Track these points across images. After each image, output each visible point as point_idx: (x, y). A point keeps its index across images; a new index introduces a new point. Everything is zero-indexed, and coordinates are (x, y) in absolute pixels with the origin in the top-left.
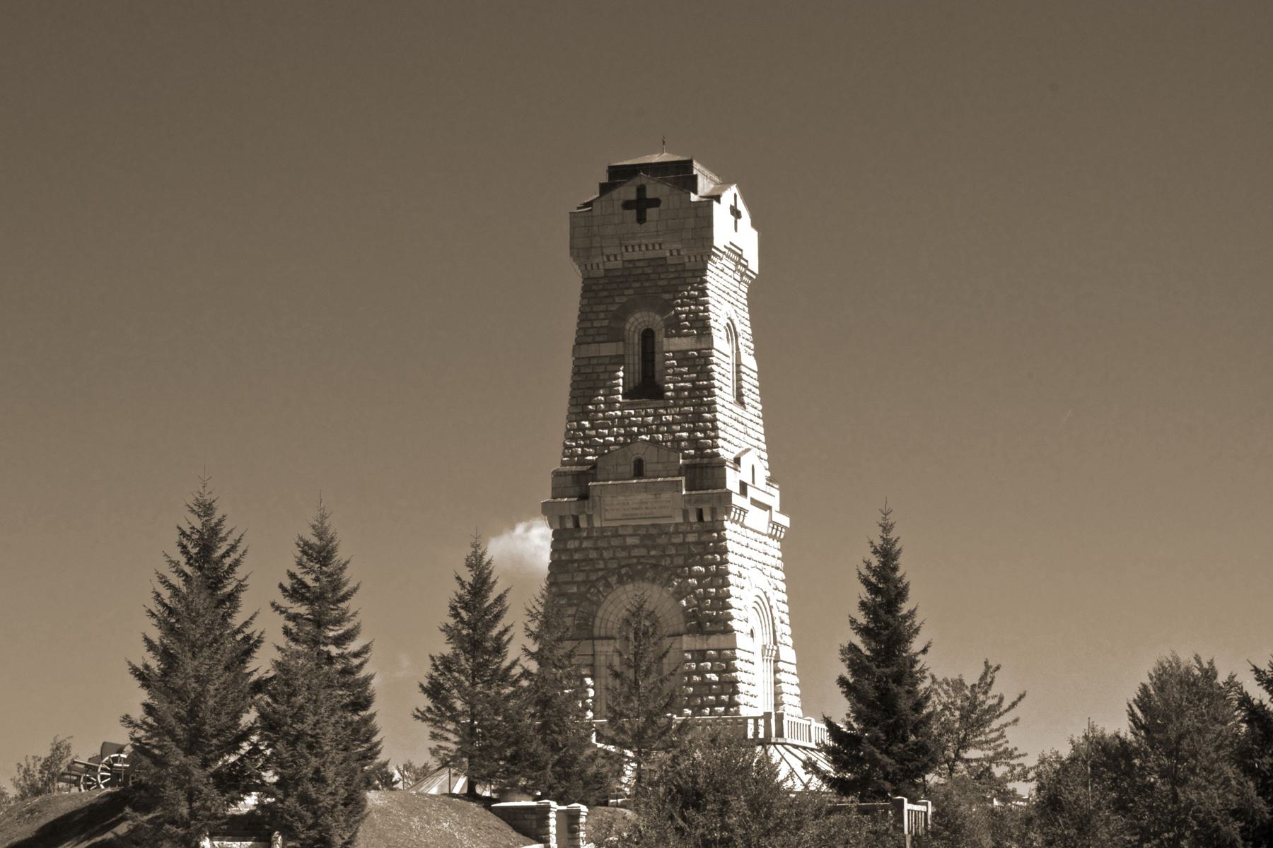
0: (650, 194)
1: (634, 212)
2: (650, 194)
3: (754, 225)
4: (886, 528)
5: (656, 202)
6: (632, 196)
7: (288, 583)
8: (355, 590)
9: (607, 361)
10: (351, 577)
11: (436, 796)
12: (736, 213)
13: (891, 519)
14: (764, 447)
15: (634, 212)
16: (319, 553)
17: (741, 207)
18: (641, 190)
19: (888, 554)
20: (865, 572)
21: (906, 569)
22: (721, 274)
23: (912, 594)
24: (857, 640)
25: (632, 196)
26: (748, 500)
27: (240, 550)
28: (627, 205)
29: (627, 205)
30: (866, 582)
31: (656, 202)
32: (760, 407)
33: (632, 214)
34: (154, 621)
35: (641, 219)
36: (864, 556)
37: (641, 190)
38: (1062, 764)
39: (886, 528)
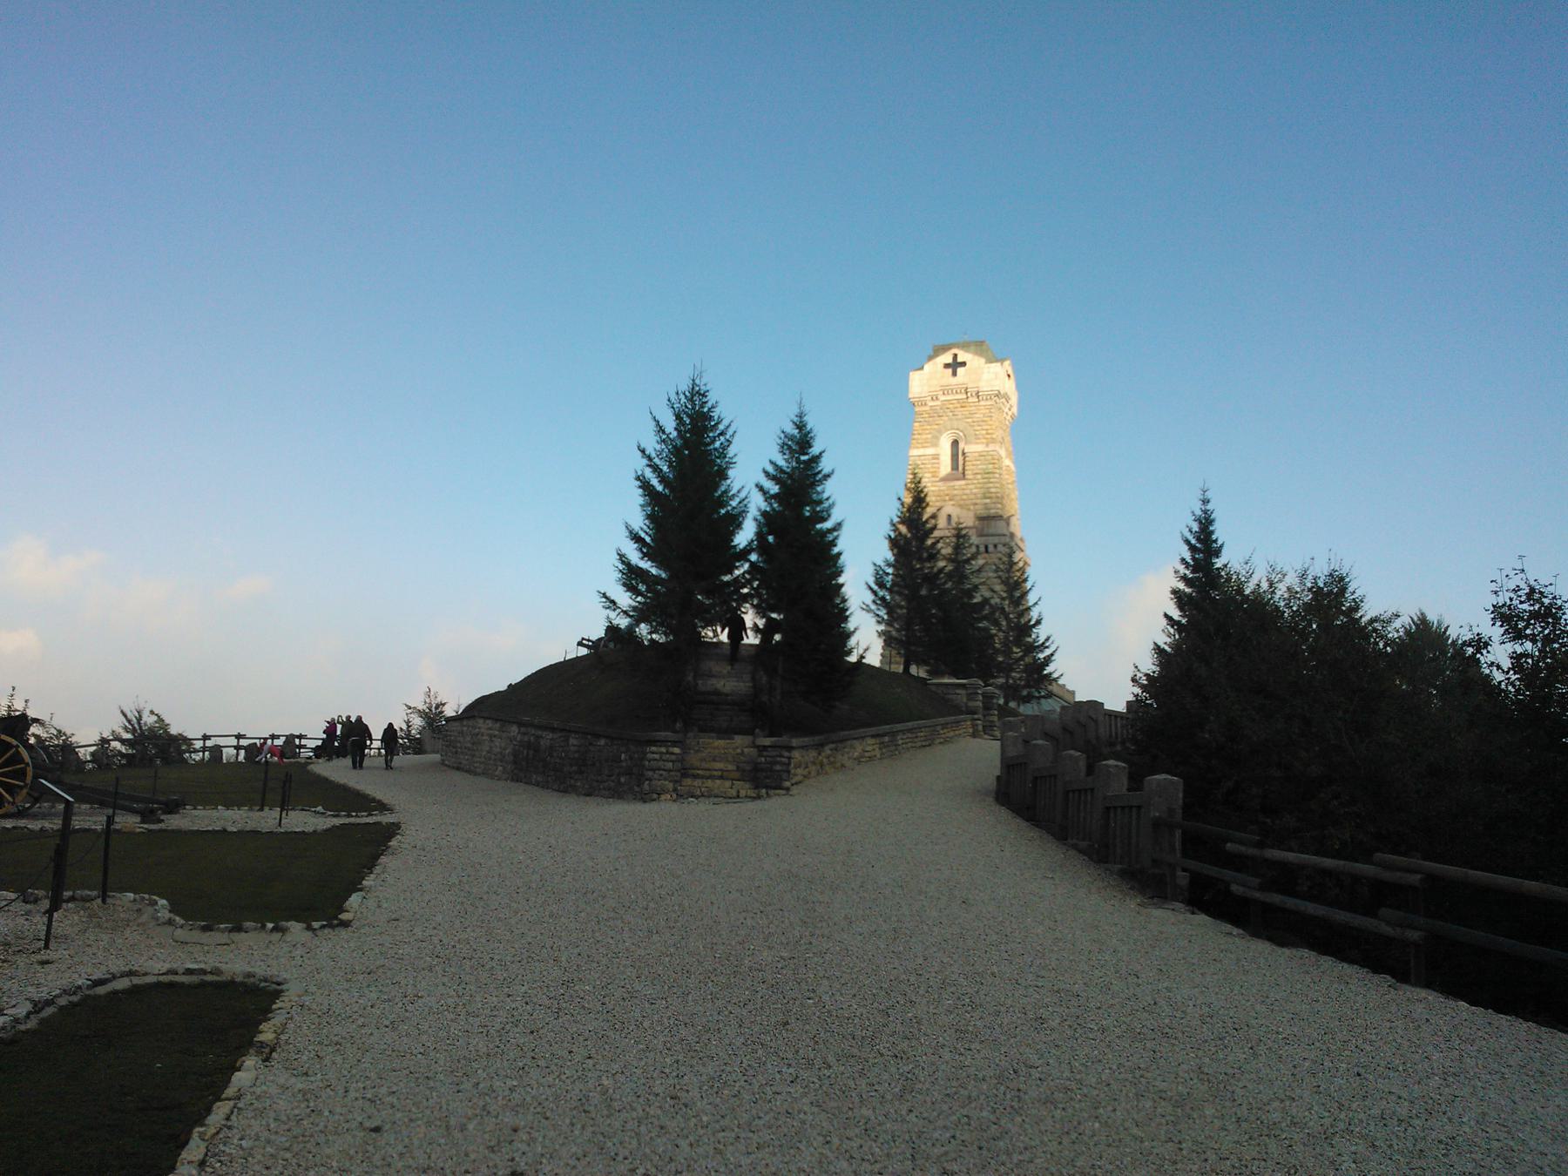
0: (960, 359)
2: (960, 359)
4: (1205, 502)
5: (963, 364)
6: (950, 360)
7: (770, 469)
10: (825, 465)
13: (1209, 495)
16: (800, 442)
18: (955, 356)
19: (1205, 524)
21: (1220, 533)
23: (1224, 551)
24: (1181, 586)
25: (950, 360)
27: (730, 432)
29: (947, 366)
30: (1187, 542)
31: (963, 364)
33: (950, 371)
35: (954, 374)
36: (1185, 523)
39: (1205, 502)
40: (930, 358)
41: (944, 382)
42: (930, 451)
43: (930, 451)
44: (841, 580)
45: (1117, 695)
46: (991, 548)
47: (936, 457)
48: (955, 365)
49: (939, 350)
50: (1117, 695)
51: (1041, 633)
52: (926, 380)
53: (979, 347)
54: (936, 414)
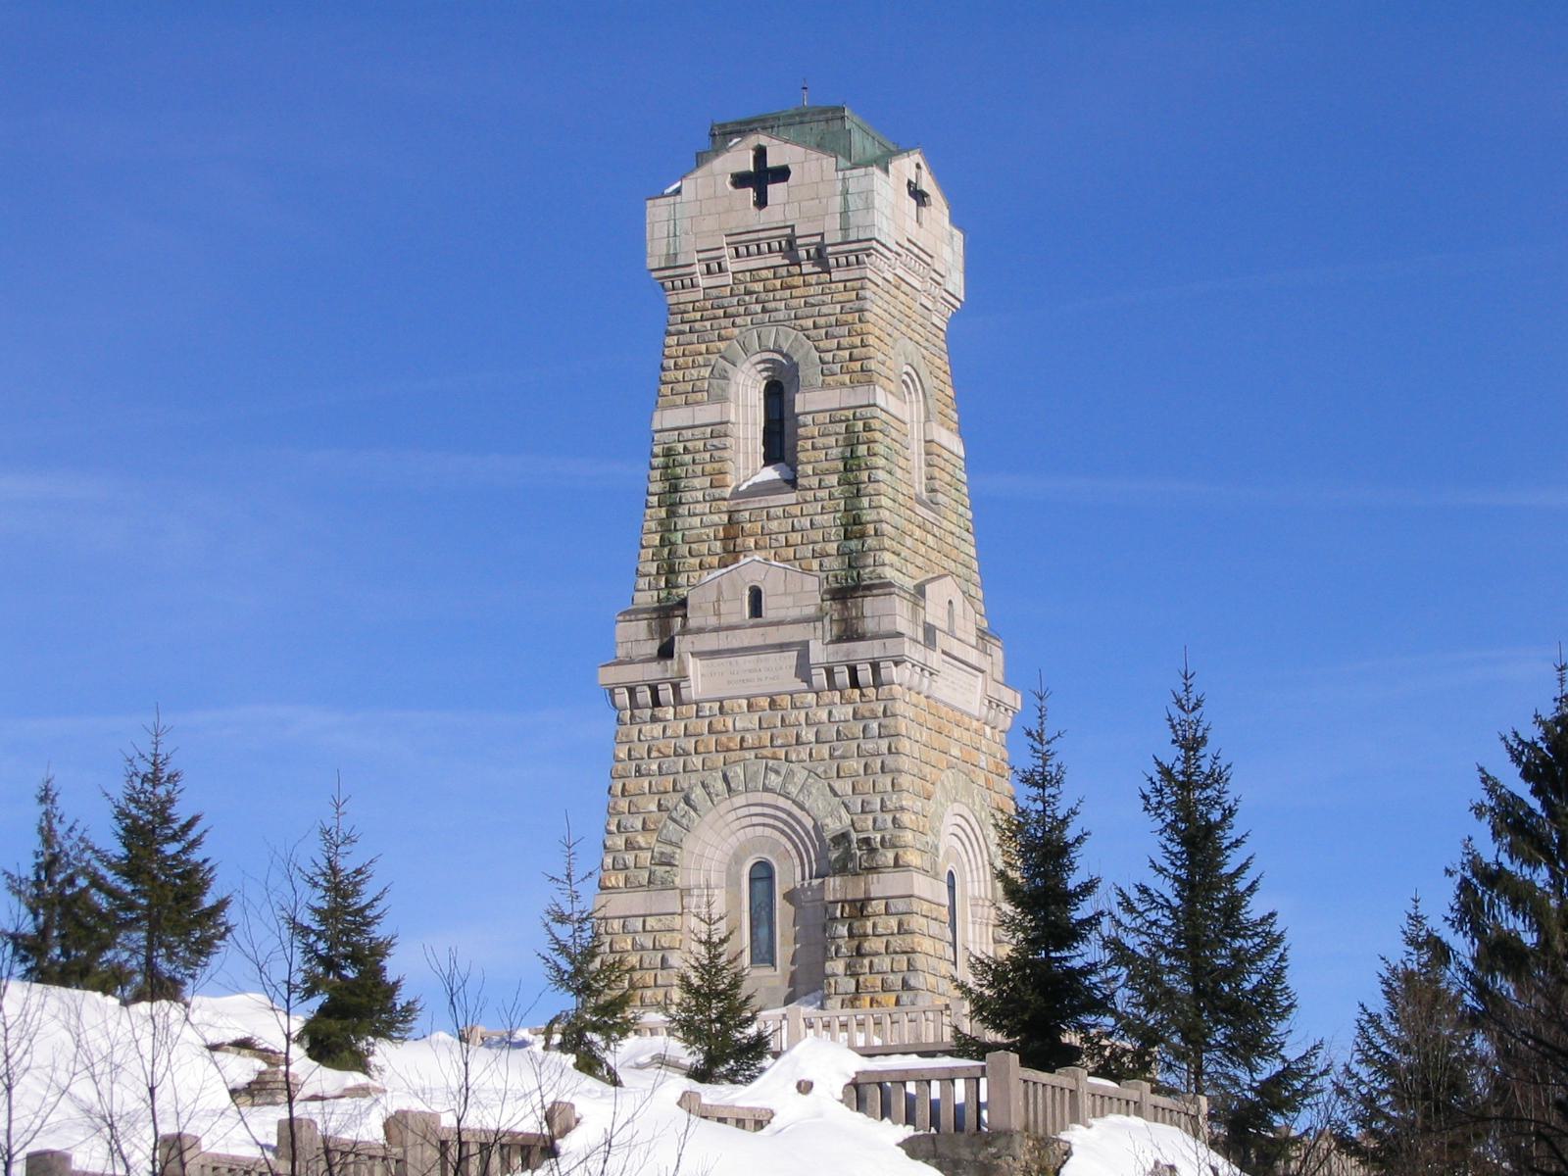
1: (771, 188)
3: (955, 221)
4: (1192, 745)
5: (782, 174)
8: (1198, 840)
9: (825, 418)
11: (1275, 1160)
12: (919, 196)
14: (976, 578)
15: (771, 188)
17: (927, 184)
18: (761, 154)
20: (1386, 974)
22: (894, 291)
26: (939, 651)
28: (740, 180)
29: (740, 180)
31: (782, 174)
32: (970, 515)
33: (750, 193)
34: (1404, 937)
35: (761, 202)
37: (761, 154)
38: (126, 857)
40: (701, 159)
41: (736, 223)
42: (707, 414)
43: (707, 414)
44: (379, 932)
45: (574, 1056)
46: (865, 674)
47: (719, 430)
48: (761, 178)
49: (722, 136)
50: (574, 1056)
51: (1254, 909)
52: (695, 215)
53: (823, 126)
54: (719, 310)
